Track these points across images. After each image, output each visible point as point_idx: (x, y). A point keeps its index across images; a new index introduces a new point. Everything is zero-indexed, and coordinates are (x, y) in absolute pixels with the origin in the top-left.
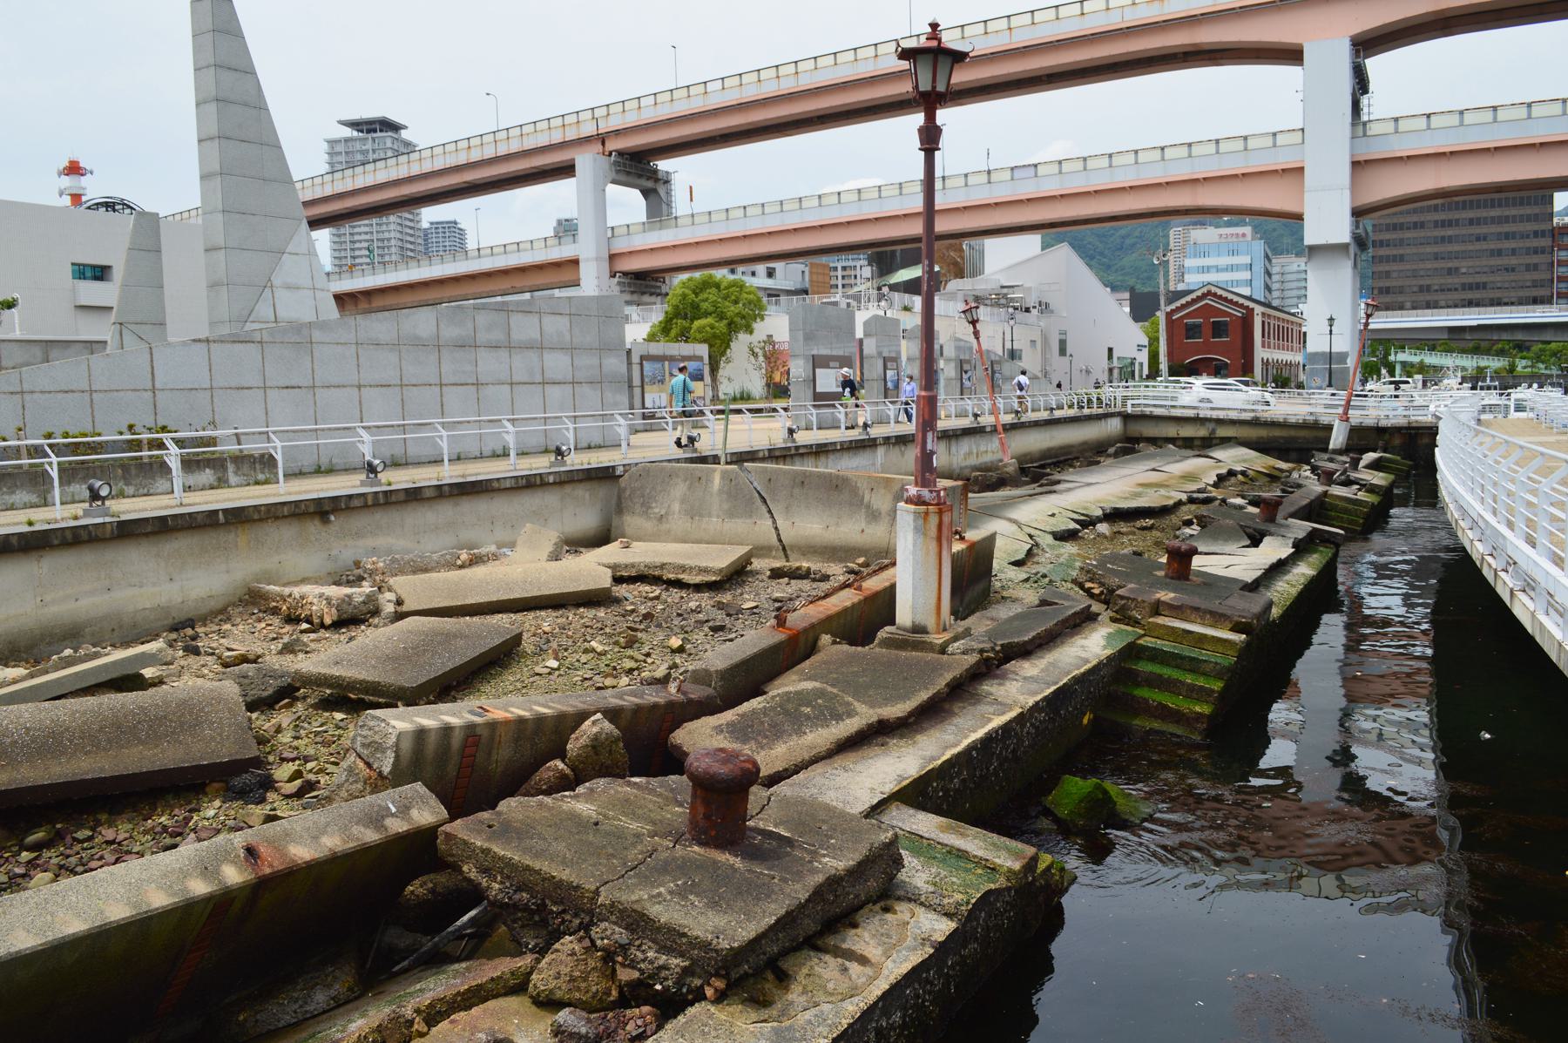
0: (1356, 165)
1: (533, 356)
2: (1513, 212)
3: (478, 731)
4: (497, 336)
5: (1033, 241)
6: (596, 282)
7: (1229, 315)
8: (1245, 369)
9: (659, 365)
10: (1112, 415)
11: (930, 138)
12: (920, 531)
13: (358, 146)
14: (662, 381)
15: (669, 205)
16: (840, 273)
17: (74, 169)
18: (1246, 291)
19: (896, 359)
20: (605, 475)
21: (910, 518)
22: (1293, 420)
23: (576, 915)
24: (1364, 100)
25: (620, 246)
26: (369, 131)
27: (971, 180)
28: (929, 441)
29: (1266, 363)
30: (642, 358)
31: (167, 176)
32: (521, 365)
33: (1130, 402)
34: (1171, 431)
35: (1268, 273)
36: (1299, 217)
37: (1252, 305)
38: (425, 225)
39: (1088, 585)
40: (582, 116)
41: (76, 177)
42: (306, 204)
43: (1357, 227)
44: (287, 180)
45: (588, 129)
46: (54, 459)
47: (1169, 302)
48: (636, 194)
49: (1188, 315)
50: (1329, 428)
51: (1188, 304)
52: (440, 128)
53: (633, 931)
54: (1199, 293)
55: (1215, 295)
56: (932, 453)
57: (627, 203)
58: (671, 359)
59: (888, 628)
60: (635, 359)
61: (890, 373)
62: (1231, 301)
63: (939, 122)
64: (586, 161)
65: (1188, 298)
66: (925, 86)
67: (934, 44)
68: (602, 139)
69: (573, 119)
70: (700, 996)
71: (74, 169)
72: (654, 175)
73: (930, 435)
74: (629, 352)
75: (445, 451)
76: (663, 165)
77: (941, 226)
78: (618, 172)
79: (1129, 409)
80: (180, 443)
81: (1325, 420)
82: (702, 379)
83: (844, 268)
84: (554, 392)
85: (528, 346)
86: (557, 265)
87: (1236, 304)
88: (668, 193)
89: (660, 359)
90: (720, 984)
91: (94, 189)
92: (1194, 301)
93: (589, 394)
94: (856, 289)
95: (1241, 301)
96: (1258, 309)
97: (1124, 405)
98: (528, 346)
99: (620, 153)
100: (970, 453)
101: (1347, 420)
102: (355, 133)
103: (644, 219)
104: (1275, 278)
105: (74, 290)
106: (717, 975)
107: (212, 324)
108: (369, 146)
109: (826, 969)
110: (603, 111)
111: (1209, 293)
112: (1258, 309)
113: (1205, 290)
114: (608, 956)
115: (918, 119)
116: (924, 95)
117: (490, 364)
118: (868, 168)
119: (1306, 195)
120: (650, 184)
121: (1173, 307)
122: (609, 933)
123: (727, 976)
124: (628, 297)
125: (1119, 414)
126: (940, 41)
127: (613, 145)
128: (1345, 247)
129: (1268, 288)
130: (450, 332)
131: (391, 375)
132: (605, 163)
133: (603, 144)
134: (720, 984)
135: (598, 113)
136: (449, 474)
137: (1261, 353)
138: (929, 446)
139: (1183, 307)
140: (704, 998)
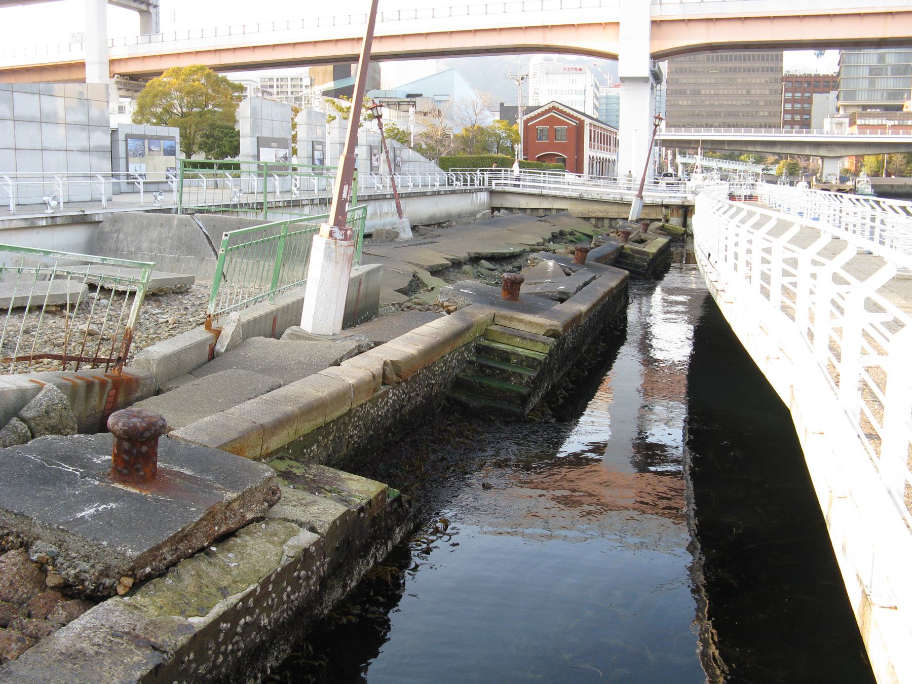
0: (654, 23)
1: (33, 127)
2: (757, 65)
7: (567, 124)
9: (139, 142)
10: (481, 190)
14: (142, 155)
16: (289, 83)
19: (322, 144)
23: (18, 536)
25: (119, 53)
29: (592, 159)
33: (494, 182)
34: (523, 203)
37: (583, 118)
43: (654, 67)
47: (526, 112)
48: (136, 15)
49: (539, 123)
51: (539, 115)
54: (547, 108)
55: (558, 109)
58: (151, 138)
60: (121, 136)
61: (317, 154)
62: (568, 115)
74: (114, 132)
79: (494, 187)
81: (627, 198)
82: (174, 154)
87: (572, 116)
89: (142, 137)
90: (128, 581)
93: (82, 162)
94: (300, 94)
95: (576, 114)
96: (587, 121)
97: (490, 184)
101: (641, 198)
111: (554, 108)
113: (551, 105)
114: (41, 566)
120: (144, 7)
121: (528, 116)
123: (133, 576)
124: (123, 93)
125: (486, 190)
128: (645, 80)
137: (588, 152)
140: (116, 594)
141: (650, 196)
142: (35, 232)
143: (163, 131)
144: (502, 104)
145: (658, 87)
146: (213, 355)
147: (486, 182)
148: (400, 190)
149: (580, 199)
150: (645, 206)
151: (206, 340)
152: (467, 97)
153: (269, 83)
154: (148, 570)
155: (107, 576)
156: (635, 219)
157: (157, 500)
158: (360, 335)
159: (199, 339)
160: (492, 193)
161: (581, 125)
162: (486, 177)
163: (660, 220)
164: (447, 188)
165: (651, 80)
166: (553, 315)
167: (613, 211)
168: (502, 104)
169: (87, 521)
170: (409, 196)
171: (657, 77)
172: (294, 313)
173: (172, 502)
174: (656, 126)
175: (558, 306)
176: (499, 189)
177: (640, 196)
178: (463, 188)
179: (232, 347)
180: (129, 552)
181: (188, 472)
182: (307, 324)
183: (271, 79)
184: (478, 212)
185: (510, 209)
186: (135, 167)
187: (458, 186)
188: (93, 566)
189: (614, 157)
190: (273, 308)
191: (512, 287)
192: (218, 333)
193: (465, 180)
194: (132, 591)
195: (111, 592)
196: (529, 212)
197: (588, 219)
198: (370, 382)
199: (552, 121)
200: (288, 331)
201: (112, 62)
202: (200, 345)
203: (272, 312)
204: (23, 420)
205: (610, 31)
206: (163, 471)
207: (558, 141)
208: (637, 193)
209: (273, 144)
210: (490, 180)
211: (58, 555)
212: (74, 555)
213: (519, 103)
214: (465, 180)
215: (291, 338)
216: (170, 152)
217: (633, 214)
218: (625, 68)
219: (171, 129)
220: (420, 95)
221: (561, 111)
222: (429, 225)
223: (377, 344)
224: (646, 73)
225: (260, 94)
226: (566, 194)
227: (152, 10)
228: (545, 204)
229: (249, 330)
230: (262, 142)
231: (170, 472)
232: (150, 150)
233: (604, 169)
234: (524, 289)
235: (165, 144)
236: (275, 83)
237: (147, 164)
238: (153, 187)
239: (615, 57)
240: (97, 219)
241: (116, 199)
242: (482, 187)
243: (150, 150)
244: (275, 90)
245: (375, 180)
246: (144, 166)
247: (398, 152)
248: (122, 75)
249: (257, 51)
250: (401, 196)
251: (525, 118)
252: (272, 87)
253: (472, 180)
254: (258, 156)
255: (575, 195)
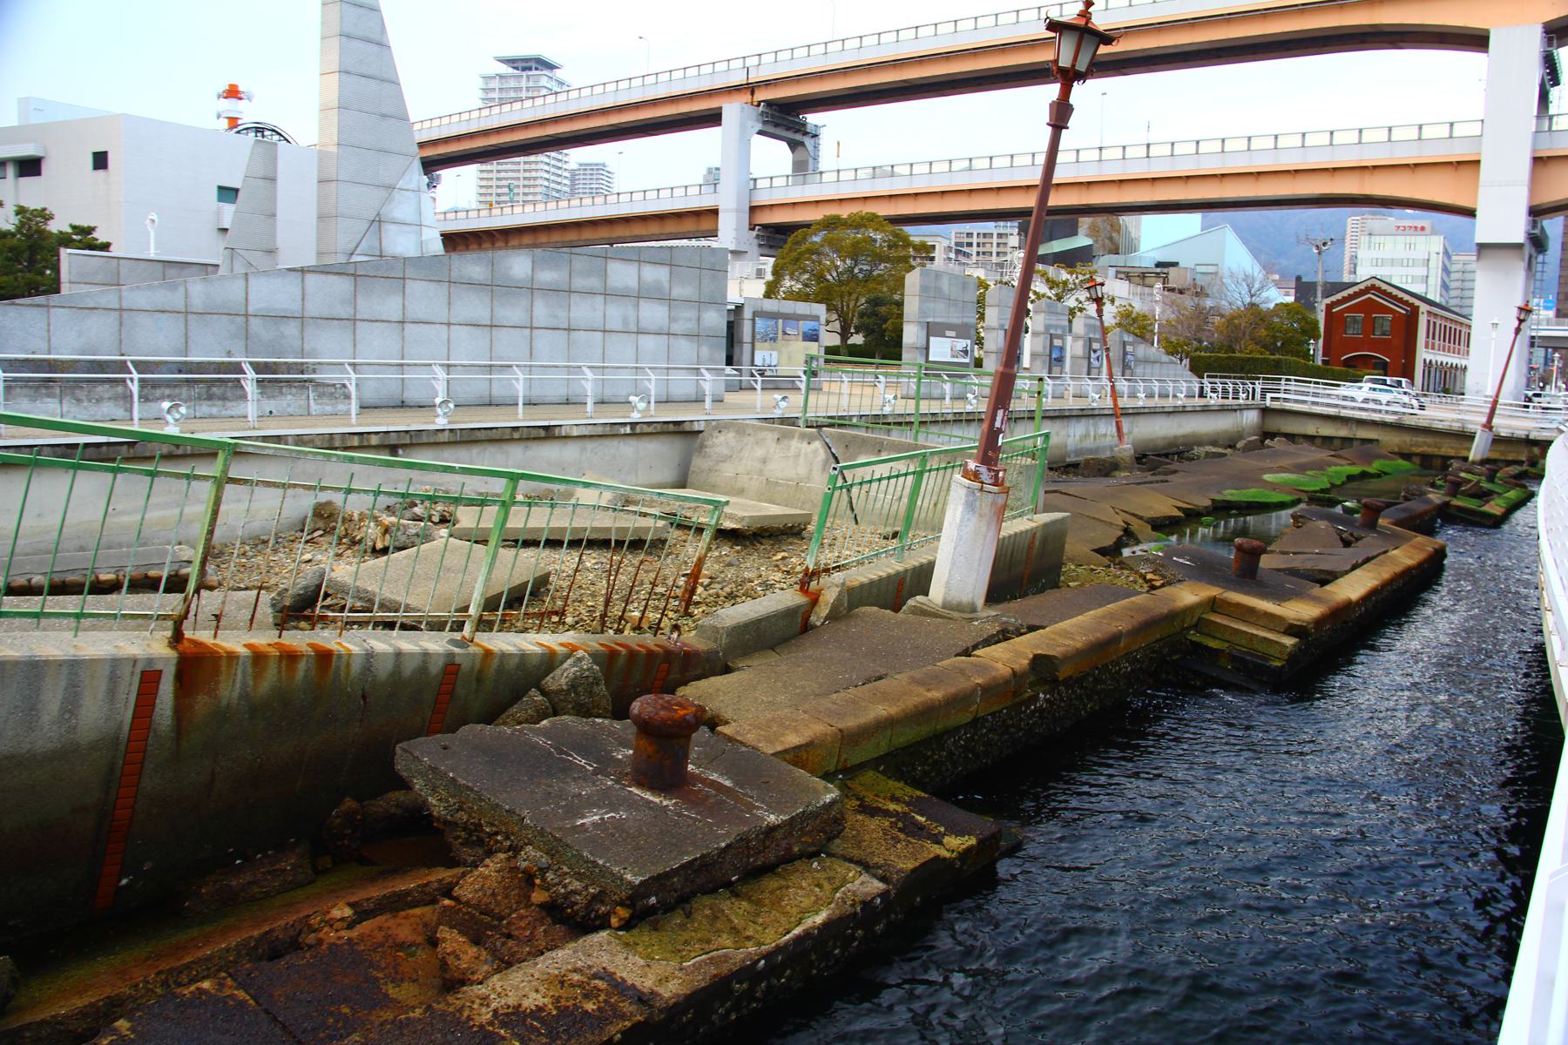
0: (1538, 161)
3: (458, 660)
4: (594, 283)
5: (1193, 220)
6: (734, 234)
8: (1408, 372)
9: (772, 323)
10: (1248, 407)
11: (1061, 115)
12: (970, 506)
13: (513, 84)
14: (774, 339)
15: (815, 159)
17: (233, 93)
18: (1418, 289)
20: (678, 430)
21: (963, 492)
22: (1440, 426)
23: (507, 838)
24: (1554, 93)
25: (762, 199)
26: (524, 69)
27: (996, 163)
28: (999, 418)
29: (1428, 365)
30: (755, 314)
31: (300, 103)
32: (616, 314)
33: (1269, 395)
34: (1311, 428)
35: (1445, 270)
36: (1471, 213)
37: (1417, 303)
38: (573, 165)
39: (1149, 576)
40: (733, 64)
41: (234, 101)
42: (422, 145)
44: (403, 117)
45: (738, 78)
46: (136, 376)
47: (1326, 295)
49: (1348, 309)
50: (1470, 437)
51: (1351, 297)
52: (592, 76)
53: (552, 856)
54: (1362, 287)
55: (1379, 289)
56: (1000, 431)
57: (772, 156)
58: (787, 317)
59: (919, 598)
60: (747, 314)
62: (1395, 298)
63: (1072, 100)
64: (732, 110)
65: (1351, 291)
66: (1065, 62)
67: (1082, 22)
68: (751, 88)
69: (724, 66)
70: (605, 925)
71: (233, 93)
72: (801, 128)
73: (1000, 413)
75: (521, 395)
76: (812, 119)
77: (1055, 200)
78: (765, 123)
79: (1268, 403)
80: (257, 368)
81: (1471, 427)
83: (1000, 235)
84: (648, 342)
85: (622, 295)
86: (697, 214)
87: (1401, 300)
88: (816, 147)
90: (624, 913)
91: (249, 113)
92: (1356, 295)
93: (685, 348)
95: (1406, 297)
96: (1424, 308)
97: (1263, 398)
98: (622, 295)
99: (769, 103)
100: (1086, 436)
101: (1491, 428)
102: (511, 71)
103: (790, 172)
104: (1454, 276)
105: (219, 213)
106: (622, 904)
107: (320, 254)
108: (524, 84)
109: (736, 910)
110: (755, 60)
111: (1373, 287)
112: (1424, 308)
113: (1369, 283)
114: (529, 878)
115: (1052, 91)
116: (1062, 71)
117: (584, 311)
118: (996, 136)
119: (1481, 190)
120: (798, 137)
121: (1334, 298)
122: (532, 855)
124: (766, 251)
126: (1088, 20)
127: (761, 95)
128: (1519, 246)
129: (1445, 286)
130: (547, 276)
131: (483, 314)
132: (753, 112)
133: (753, 94)
134: (624, 913)
135: (749, 62)
136: (522, 418)
137: (1423, 354)
138: (998, 424)
139: (1345, 300)
140: (609, 926)
141: (1507, 424)
142: (615, 443)
143: (802, 308)
144: (1298, 278)
145: (1540, 258)
146: (806, 627)
147: (1258, 396)
148: (1124, 402)
149: (1398, 427)
150: (1498, 441)
151: (798, 607)
152: (1236, 266)
153: (966, 240)
154: (653, 900)
155: (602, 902)
156: (1478, 458)
157: (680, 815)
158: (1011, 613)
159: (790, 604)
160: (1265, 411)
161: (1415, 310)
162: (1258, 387)
163: (1520, 463)
164: (1198, 402)
165: (1528, 249)
166: (1317, 600)
167: (1447, 449)
168: (1298, 278)
169: (586, 831)
170: (1137, 413)
171: (1538, 242)
172: (921, 578)
173: (696, 820)
174: (1521, 321)
175: (1316, 590)
176: (1276, 405)
177: (1488, 425)
178: (1221, 402)
179: (835, 616)
180: (629, 877)
181: (728, 783)
182: (937, 592)
183: (969, 235)
184: (1200, 444)
185: (1291, 437)
186: (763, 356)
187: (1214, 400)
188: (586, 888)
189: (1464, 362)
190: (900, 568)
191: (1250, 556)
192: (815, 601)
193: (1225, 391)
194: (627, 926)
195: (602, 924)
196: (1318, 441)
197: (1406, 456)
198: (1007, 682)
199: (1369, 307)
200: (911, 602)
201: (753, 209)
202: (790, 613)
203: (898, 573)
204: (544, 693)
205: (1465, 173)
206: (697, 778)
207: (1379, 332)
208: (1484, 420)
209: (948, 333)
210: (1264, 392)
211: (548, 868)
212: (565, 869)
213: (1320, 279)
214: (1225, 391)
215: (913, 613)
216: (812, 337)
217: (1477, 451)
218: (1487, 229)
219: (815, 305)
220: (1175, 264)
221: (1384, 292)
222: (1166, 456)
223: (1032, 629)
224: (1519, 237)
225: (952, 255)
226: (1376, 417)
227: (808, 141)
228: (1343, 432)
229: (856, 597)
230: (932, 330)
231: (705, 782)
232: (785, 333)
233: (1447, 382)
234: (1266, 562)
235: (806, 326)
236: (975, 240)
237: (780, 353)
238: (776, 383)
239: (1471, 213)
240: (696, 427)
241: (731, 398)
242: (1250, 402)
243: (785, 333)
244: (975, 249)
245: (1089, 386)
246: (775, 354)
247: (1129, 349)
248: (765, 227)
249: (948, 198)
250: (1126, 413)
251: (1328, 301)
252: (970, 245)
253: (1236, 392)
254: (927, 348)
255: (1390, 418)
